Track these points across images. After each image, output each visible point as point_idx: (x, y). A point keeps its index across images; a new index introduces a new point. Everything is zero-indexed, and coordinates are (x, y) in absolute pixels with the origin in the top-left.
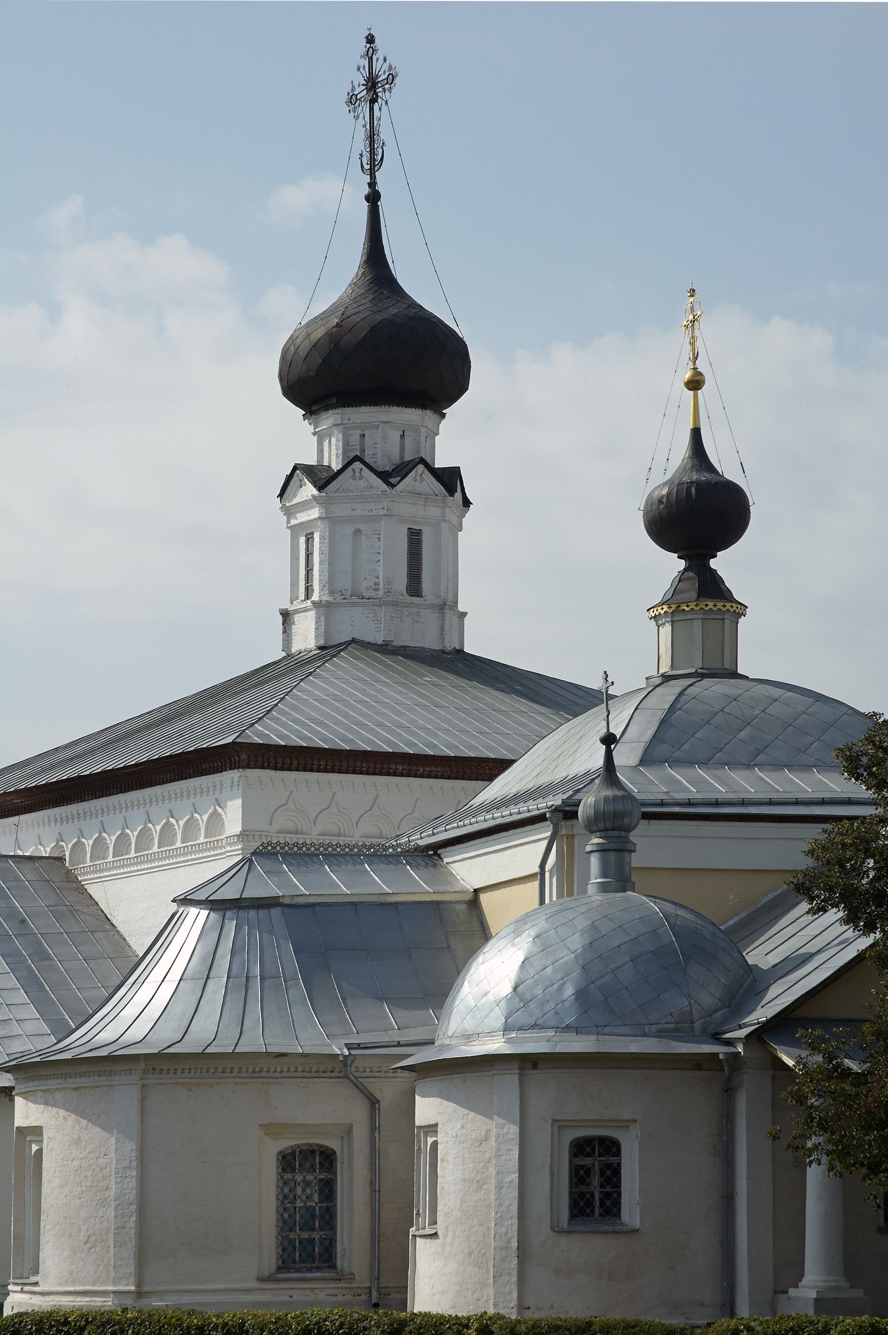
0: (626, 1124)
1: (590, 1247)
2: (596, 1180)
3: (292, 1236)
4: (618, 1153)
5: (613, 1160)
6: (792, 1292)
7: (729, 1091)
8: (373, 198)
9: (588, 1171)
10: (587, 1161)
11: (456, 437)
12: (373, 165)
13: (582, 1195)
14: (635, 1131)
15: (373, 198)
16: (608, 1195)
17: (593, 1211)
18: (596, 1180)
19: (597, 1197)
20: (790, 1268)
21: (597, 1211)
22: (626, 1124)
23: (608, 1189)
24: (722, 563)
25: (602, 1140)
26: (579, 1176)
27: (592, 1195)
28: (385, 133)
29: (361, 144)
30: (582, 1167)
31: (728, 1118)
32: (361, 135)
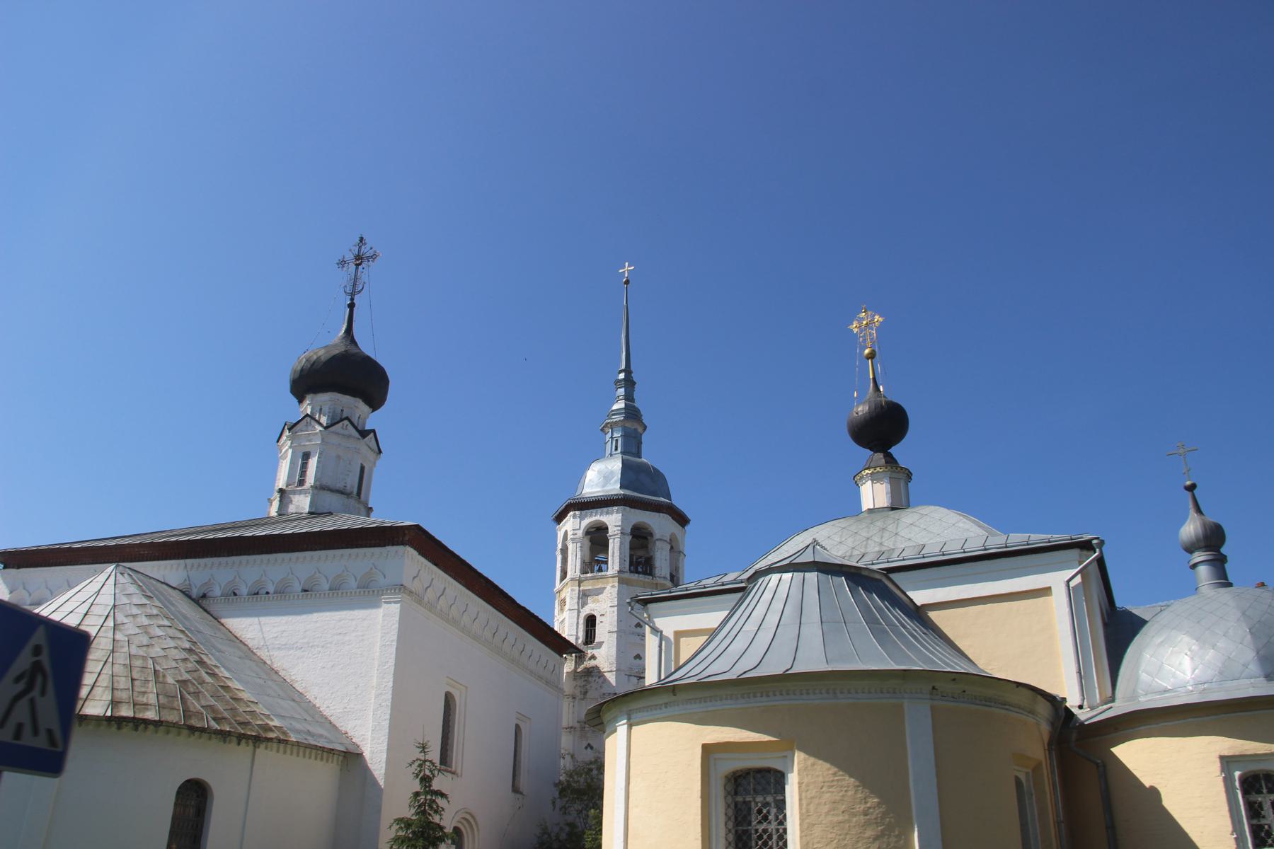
8: (352, 306)
11: (373, 420)
15: (352, 306)
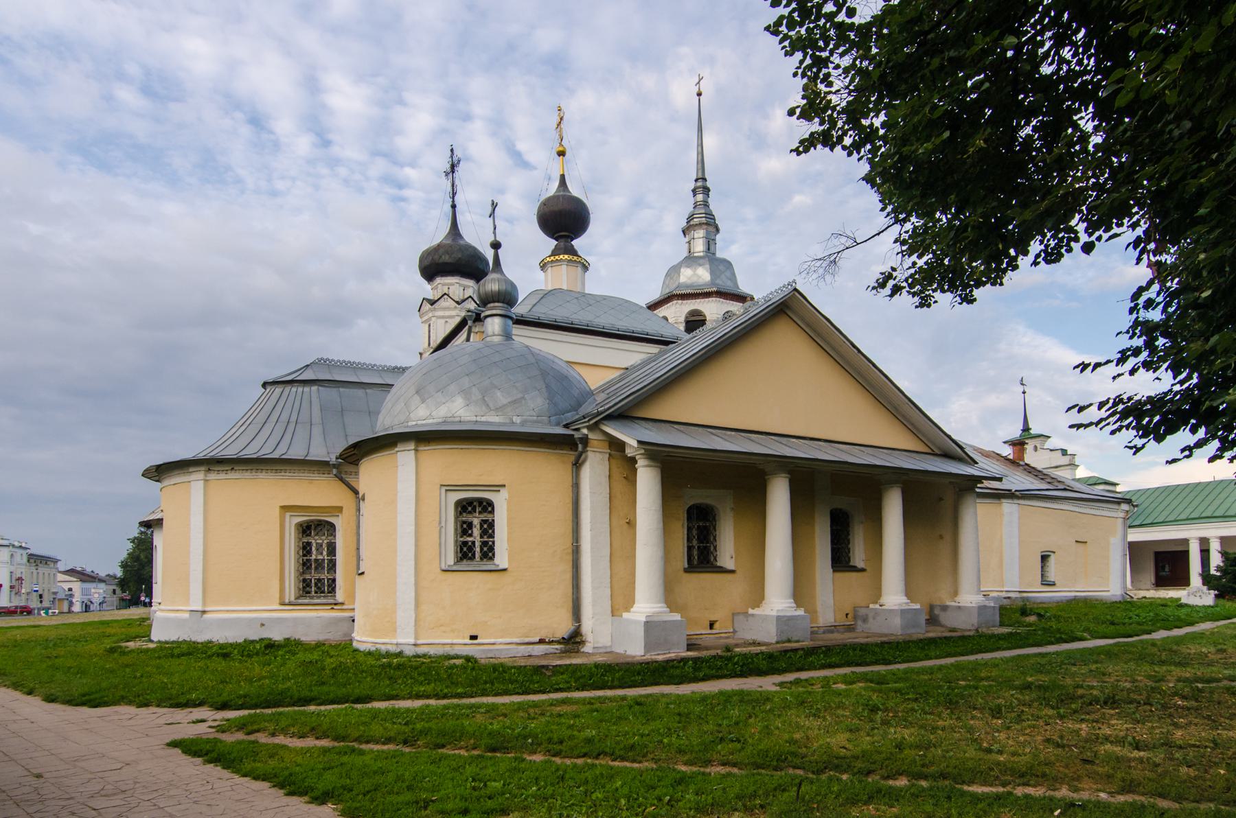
0: (497, 488)
1: (473, 583)
2: (476, 532)
3: (308, 577)
4: (492, 512)
5: (489, 517)
6: (625, 615)
7: (577, 465)
8: (454, 206)
9: (470, 525)
10: (469, 518)
12: (454, 194)
13: (465, 543)
14: (504, 493)
15: (454, 206)
16: (484, 544)
17: (474, 555)
18: (476, 532)
19: (478, 544)
20: (622, 598)
21: (478, 555)
22: (497, 488)
23: (485, 539)
24: (576, 243)
25: (480, 501)
26: (465, 529)
27: (473, 543)
28: (457, 182)
29: (449, 189)
30: (464, 522)
31: (576, 486)
32: (450, 185)
